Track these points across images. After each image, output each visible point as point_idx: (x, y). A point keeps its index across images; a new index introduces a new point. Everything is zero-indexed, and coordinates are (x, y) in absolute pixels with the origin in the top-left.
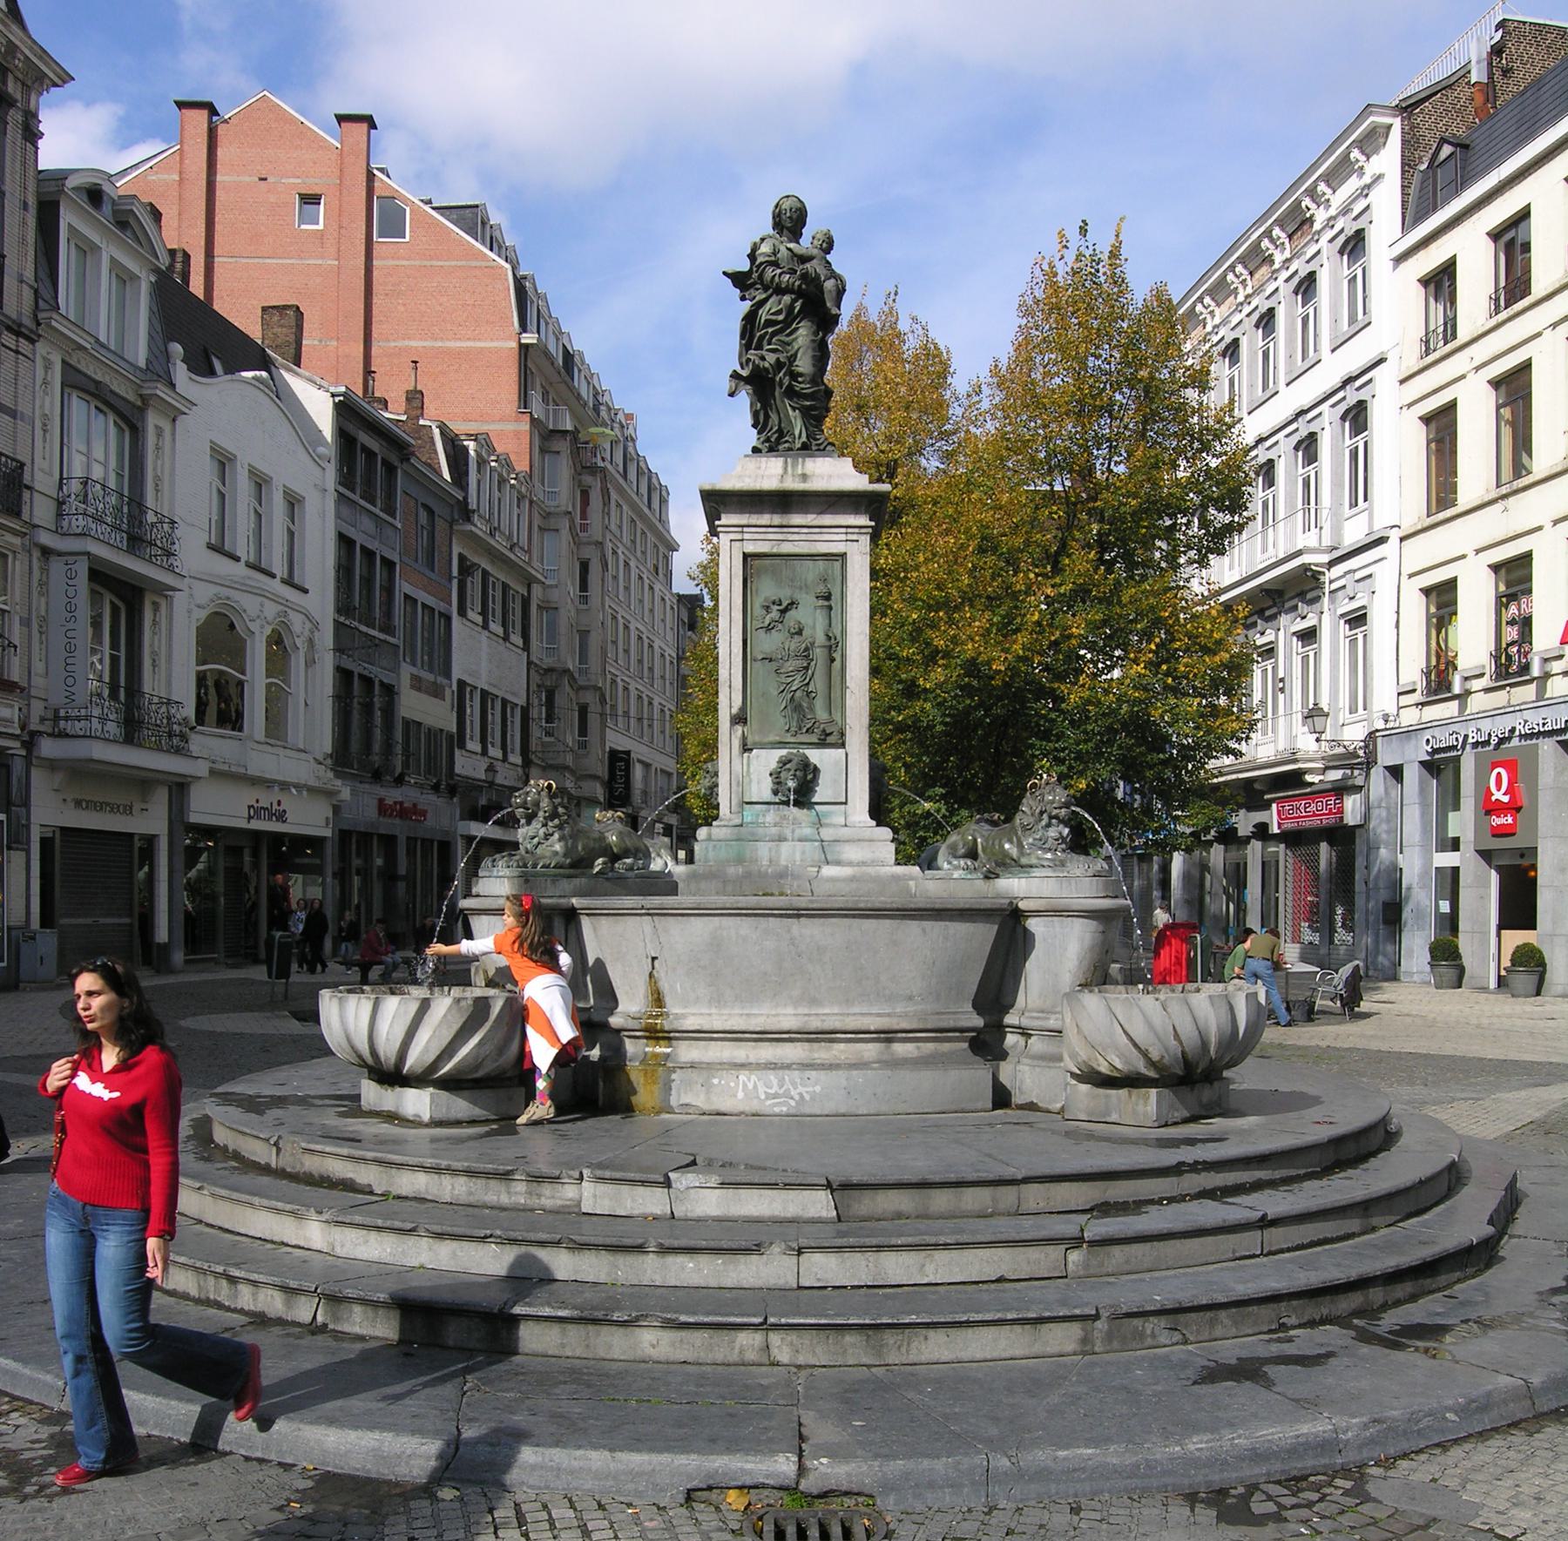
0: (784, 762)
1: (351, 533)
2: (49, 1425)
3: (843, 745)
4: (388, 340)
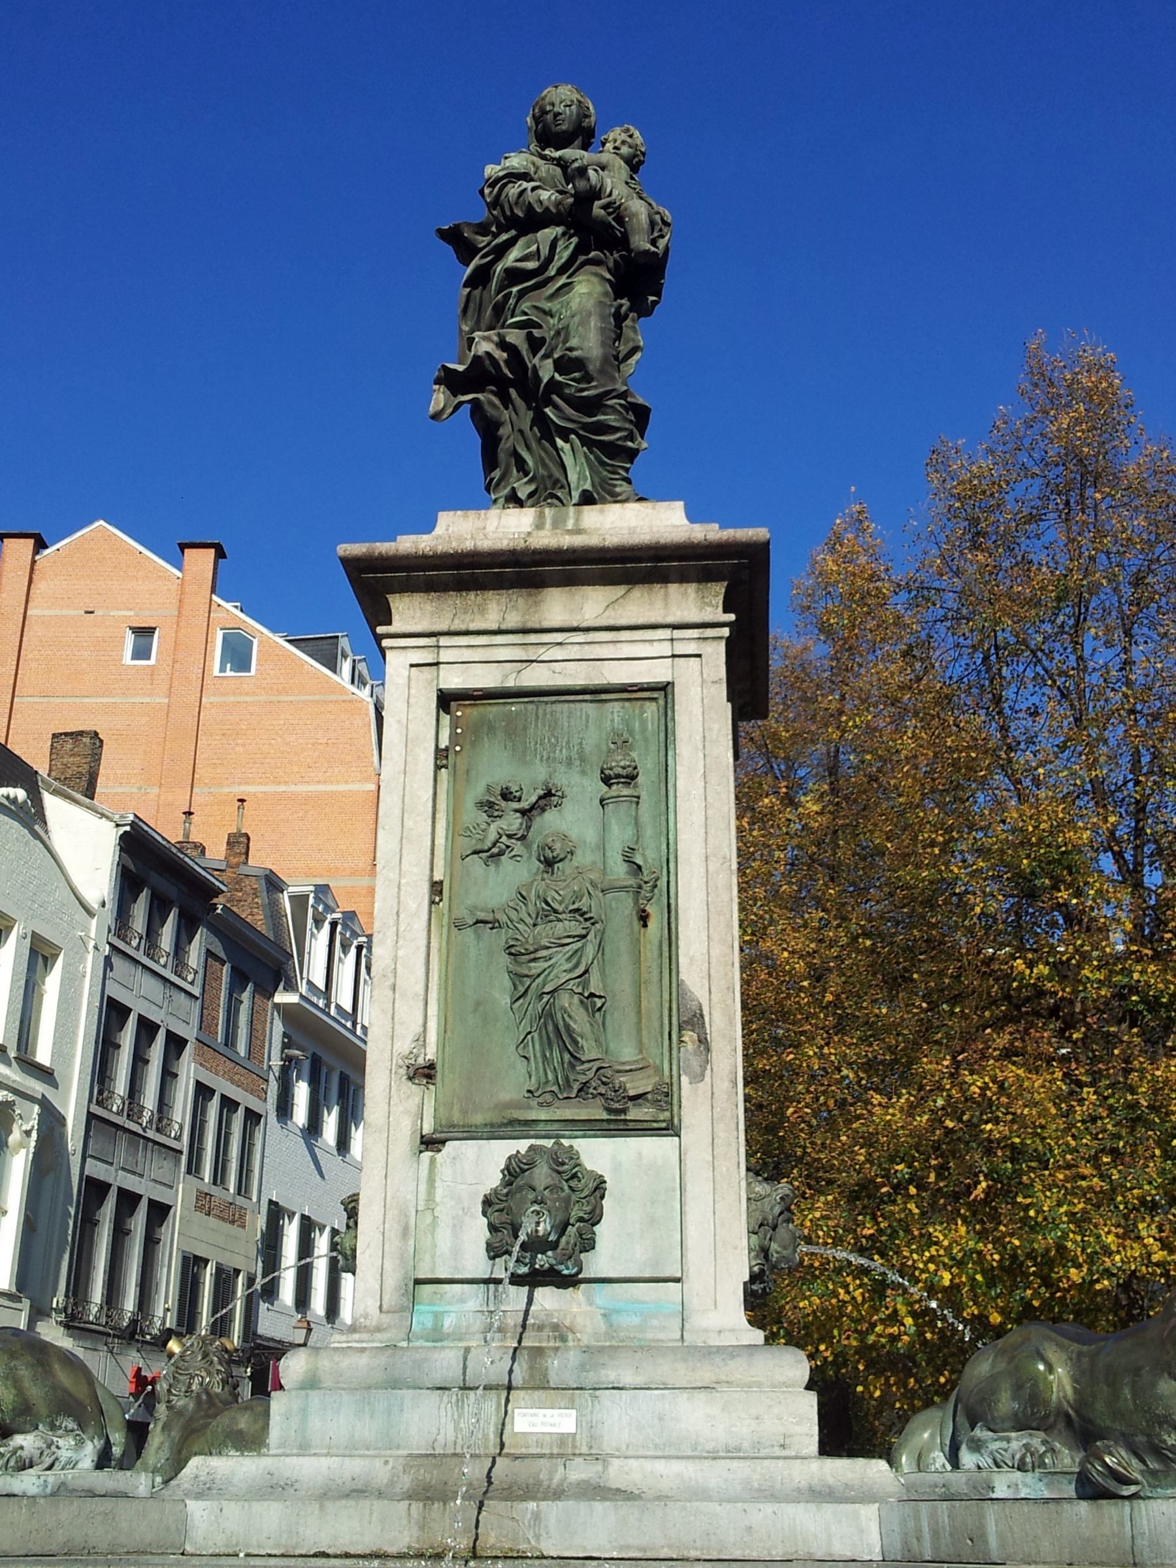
0: (515, 1171)
2: (1078, 1342)
3: (671, 1129)
4: (220, 785)
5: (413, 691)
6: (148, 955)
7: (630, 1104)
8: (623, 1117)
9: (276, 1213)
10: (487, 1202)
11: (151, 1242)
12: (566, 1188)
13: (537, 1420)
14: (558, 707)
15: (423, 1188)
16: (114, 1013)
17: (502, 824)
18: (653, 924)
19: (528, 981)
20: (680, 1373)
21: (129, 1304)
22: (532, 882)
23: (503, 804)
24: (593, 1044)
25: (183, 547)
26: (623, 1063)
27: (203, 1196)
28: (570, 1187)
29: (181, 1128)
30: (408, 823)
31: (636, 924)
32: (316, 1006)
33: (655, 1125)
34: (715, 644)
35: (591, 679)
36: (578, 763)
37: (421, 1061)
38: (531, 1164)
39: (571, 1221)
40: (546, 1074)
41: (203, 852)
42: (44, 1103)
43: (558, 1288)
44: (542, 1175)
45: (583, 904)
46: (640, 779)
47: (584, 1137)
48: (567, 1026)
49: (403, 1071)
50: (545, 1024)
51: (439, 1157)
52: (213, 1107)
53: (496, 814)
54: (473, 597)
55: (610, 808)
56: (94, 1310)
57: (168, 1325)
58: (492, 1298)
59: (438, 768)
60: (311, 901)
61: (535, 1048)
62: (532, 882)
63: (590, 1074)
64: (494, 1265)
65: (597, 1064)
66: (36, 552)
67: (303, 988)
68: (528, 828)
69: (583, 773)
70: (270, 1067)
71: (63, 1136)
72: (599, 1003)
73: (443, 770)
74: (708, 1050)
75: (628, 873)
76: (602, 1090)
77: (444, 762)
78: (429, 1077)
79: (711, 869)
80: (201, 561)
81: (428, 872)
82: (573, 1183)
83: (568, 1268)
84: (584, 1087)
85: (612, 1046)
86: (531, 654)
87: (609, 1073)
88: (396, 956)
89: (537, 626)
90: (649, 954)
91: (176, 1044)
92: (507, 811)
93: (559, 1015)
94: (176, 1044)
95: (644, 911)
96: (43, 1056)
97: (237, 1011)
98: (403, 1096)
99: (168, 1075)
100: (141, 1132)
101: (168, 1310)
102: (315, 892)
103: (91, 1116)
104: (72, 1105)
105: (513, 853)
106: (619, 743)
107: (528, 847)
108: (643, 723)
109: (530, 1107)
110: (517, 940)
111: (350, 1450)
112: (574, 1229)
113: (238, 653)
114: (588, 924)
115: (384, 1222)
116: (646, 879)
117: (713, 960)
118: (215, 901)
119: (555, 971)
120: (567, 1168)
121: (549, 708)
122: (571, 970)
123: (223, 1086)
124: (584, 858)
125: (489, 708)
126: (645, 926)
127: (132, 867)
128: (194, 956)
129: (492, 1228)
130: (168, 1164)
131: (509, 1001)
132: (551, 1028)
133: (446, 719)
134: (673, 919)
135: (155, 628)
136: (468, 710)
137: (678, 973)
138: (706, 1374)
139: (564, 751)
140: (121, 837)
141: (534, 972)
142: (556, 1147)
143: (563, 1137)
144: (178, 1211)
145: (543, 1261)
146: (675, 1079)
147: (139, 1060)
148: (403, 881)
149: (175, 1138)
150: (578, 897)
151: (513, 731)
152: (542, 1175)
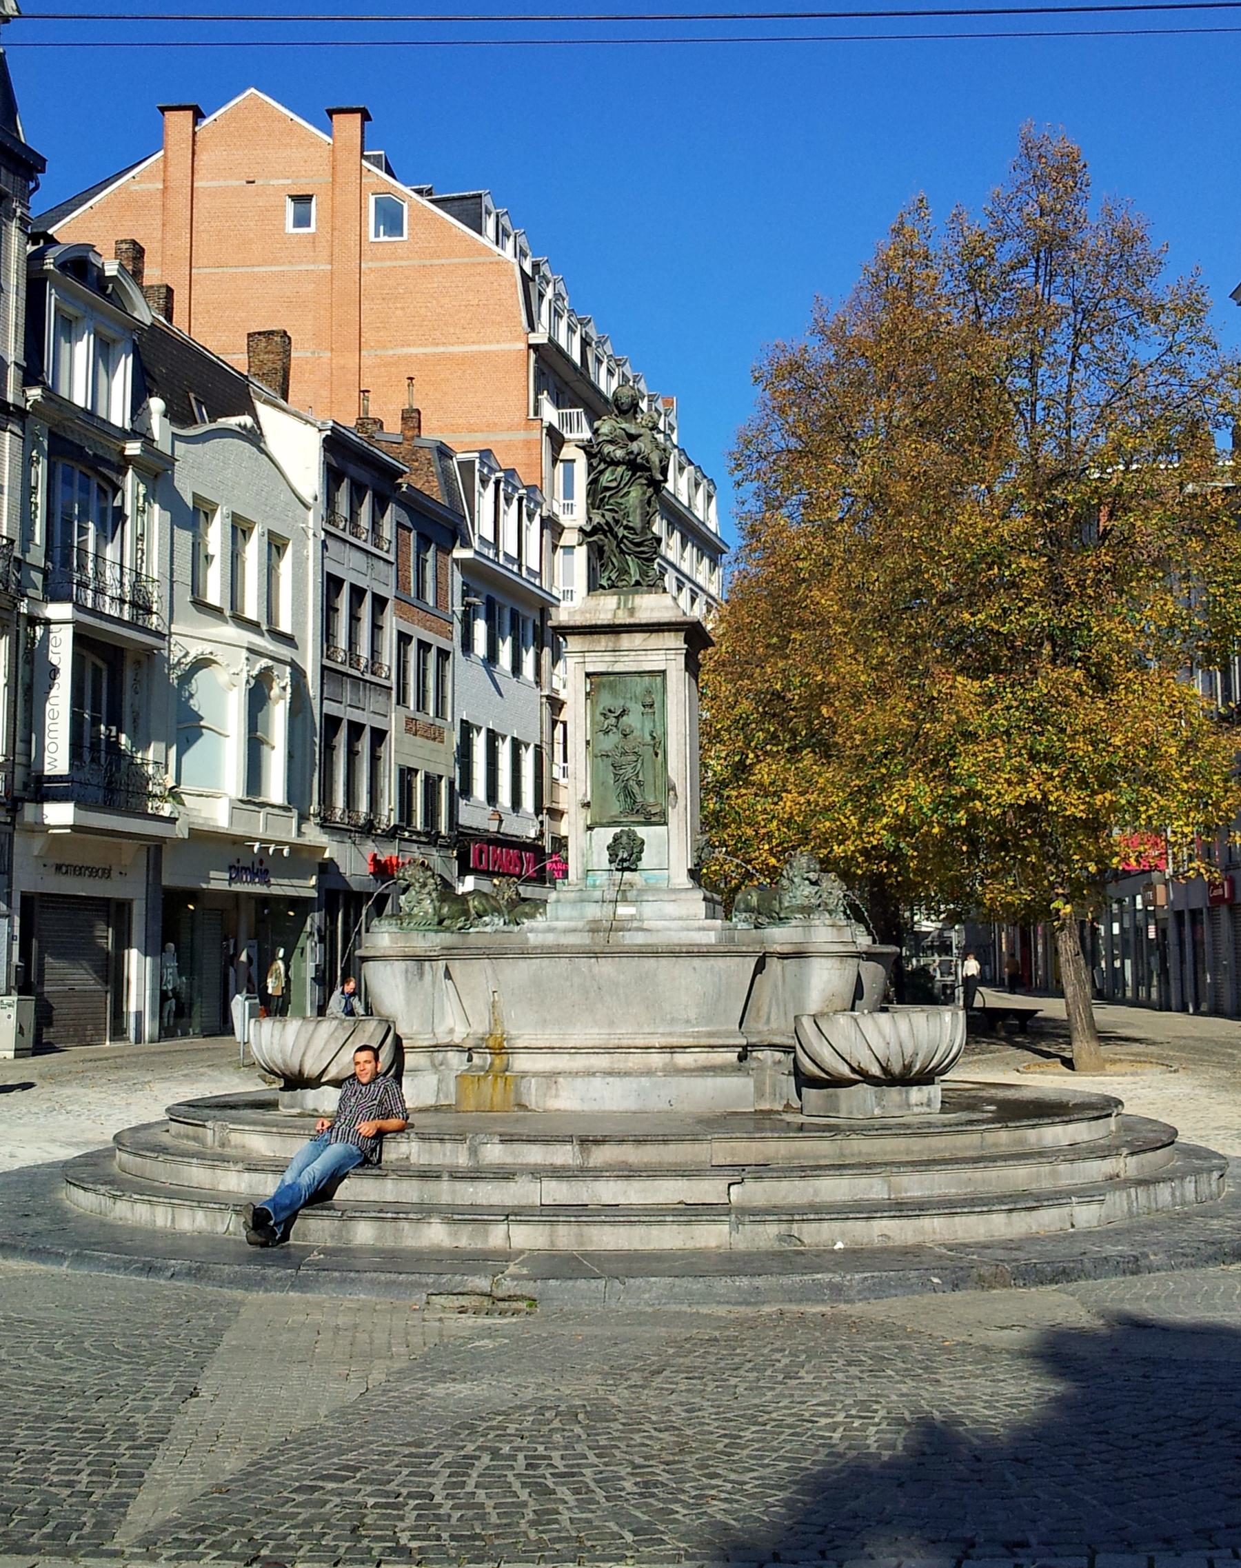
0: (616, 838)
1: (337, 571)
3: (665, 824)
4: (385, 348)
9: (467, 729)
10: (608, 848)
11: (375, 759)
13: (624, 910)
16: (332, 584)
20: (666, 897)
21: (363, 806)
25: (331, 113)
27: (410, 720)
32: (488, 558)
41: (381, 427)
42: (293, 665)
44: (624, 840)
52: (413, 649)
56: (339, 812)
60: (477, 466)
61: (622, 798)
66: (195, 124)
67: (476, 543)
70: (453, 612)
71: (305, 685)
80: (349, 125)
91: (380, 603)
94: (380, 603)
96: (285, 626)
97: (424, 568)
99: (376, 628)
100: (360, 675)
102: (480, 458)
103: (323, 668)
104: (310, 664)
111: (571, 919)
113: (390, 218)
118: (400, 481)
120: (632, 837)
123: (418, 632)
128: (387, 530)
138: (673, 897)
140: (324, 440)
144: (393, 734)
145: (625, 865)
147: (354, 619)
151: (612, 687)
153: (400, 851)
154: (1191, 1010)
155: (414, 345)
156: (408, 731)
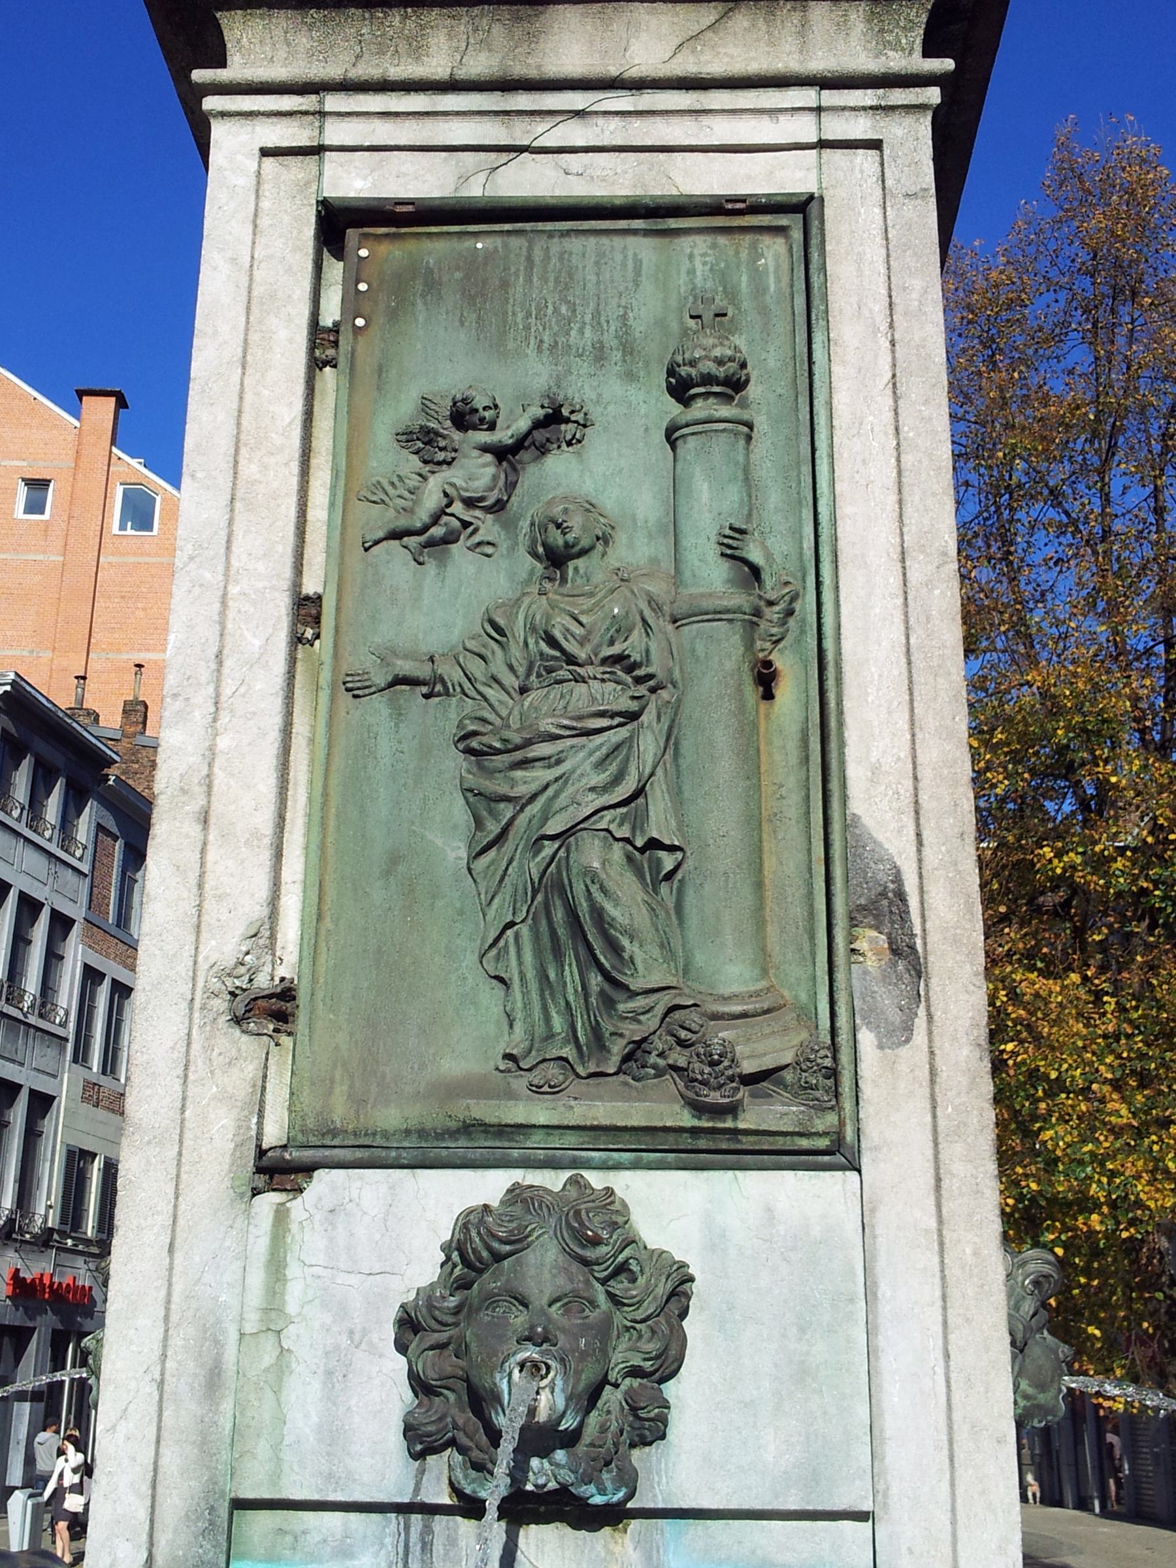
0: (476, 1255)
3: (840, 1154)
4: (119, 651)
5: (265, 204)
6: (31, 827)
7: (743, 1093)
8: (729, 1124)
10: (409, 1325)
12: (602, 1298)
14: (575, 244)
15: (257, 1278)
17: (455, 476)
18: (787, 691)
19: (507, 811)
22: (518, 601)
23: (457, 436)
24: (656, 952)
25: (81, 394)
26: (726, 999)
28: (611, 1296)
29: (67, 1014)
30: (249, 469)
31: (751, 693)
33: (804, 1143)
34: (909, 120)
35: (644, 185)
36: (617, 356)
37: (262, 981)
38: (519, 1242)
39: (612, 1376)
40: (547, 1019)
43: (576, 1526)
44: (543, 1267)
45: (634, 645)
46: (753, 391)
47: (635, 1166)
48: (598, 914)
49: (221, 1004)
50: (547, 905)
51: (298, 1207)
53: (441, 456)
54: (397, 21)
55: (689, 447)
57: (50, 1225)
58: (415, 1548)
59: (315, 364)
61: (521, 960)
62: (518, 601)
63: (651, 1022)
64: (421, 1472)
65: (664, 1001)
68: (511, 486)
69: (630, 376)
72: (668, 861)
73: (328, 369)
74: (918, 970)
75: (730, 581)
76: (679, 1058)
77: (331, 352)
78: (282, 1017)
79: (914, 576)
80: (101, 410)
81: (288, 572)
82: (619, 1286)
83: (602, 1491)
84: (636, 1052)
85: (699, 959)
86: (520, 132)
87: (693, 1018)
88: (212, 749)
89: (533, 73)
90: (778, 757)
91: (61, 924)
92: (465, 448)
93: (579, 888)
94: (61, 924)
95: (768, 664)
98: (218, 1061)
99: (53, 957)
100: (21, 1017)
101: (51, 1207)
105: (477, 538)
106: (708, 316)
107: (510, 526)
108: (758, 277)
109: (510, 1095)
110: (484, 720)
112: (619, 1394)
114: (642, 690)
115: (164, 1356)
116: (772, 595)
117: (925, 773)
118: (106, 771)
119: (570, 790)
120: (599, 1244)
121: (556, 245)
122: (606, 788)
124: (634, 550)
125: (428, 245)
126: (768, 696)
127: (13, 730)
129: (420, 1385)
130: (52, 1052)
131: (465, 856)
132: (559, 915)
133: (335, 270)
134: (830, 683)
135: (50, 481)
136: (384, 248)
137: (844, 799)
139: (588, 332)
141: (522, 790)
142: (573, 1193)
143: (589, 1165)
144: (62, 1102)
145: (543, 1473)
146: (843, 1037)
148: (233, 590)
149: (60, 1025)
150: (621, 630)
151: (480, 292)
152: (543, 1267)
153: (56, 1265)
154: (1097, 1510)
155: (154, 650)
156: (84, 1099)
